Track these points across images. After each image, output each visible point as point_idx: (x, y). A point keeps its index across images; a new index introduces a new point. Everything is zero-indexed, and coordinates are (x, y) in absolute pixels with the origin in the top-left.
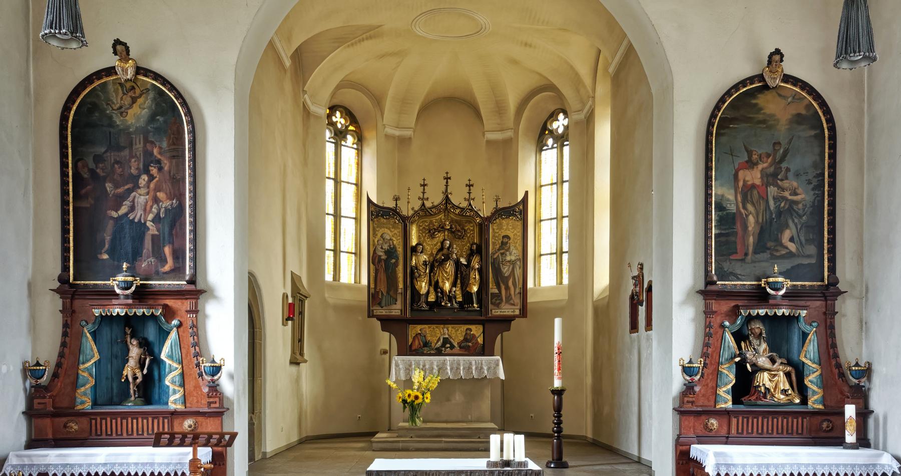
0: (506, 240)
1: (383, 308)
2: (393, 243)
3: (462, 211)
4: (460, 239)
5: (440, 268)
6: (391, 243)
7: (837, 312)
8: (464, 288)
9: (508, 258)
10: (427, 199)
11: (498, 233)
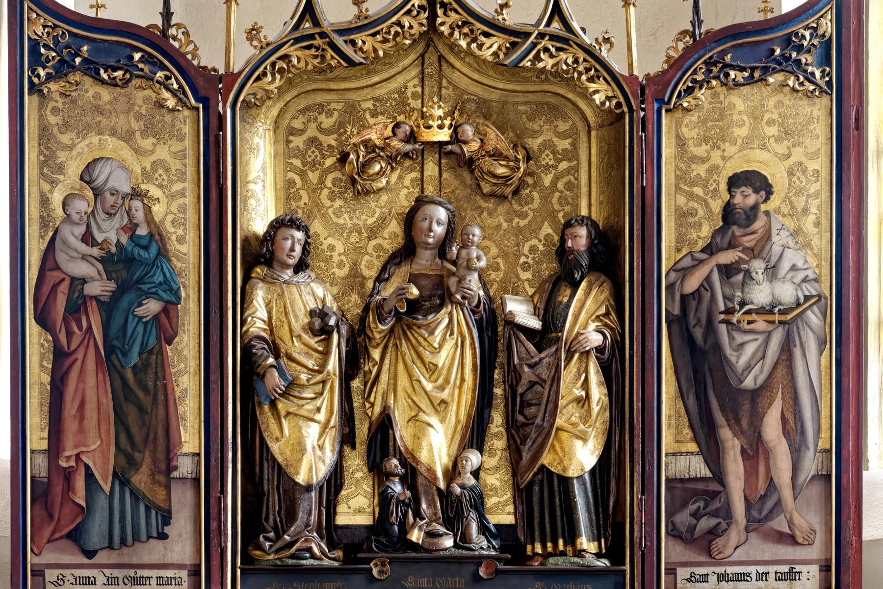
0: (745, 198)
1: (97, 560)
2: (148, 210)
3: (514, 45)
4: (503, 198)
5: (397, 347)
6: (139, 216)
7: (173, 13)
8: (526, 456)
11: (703, 160)
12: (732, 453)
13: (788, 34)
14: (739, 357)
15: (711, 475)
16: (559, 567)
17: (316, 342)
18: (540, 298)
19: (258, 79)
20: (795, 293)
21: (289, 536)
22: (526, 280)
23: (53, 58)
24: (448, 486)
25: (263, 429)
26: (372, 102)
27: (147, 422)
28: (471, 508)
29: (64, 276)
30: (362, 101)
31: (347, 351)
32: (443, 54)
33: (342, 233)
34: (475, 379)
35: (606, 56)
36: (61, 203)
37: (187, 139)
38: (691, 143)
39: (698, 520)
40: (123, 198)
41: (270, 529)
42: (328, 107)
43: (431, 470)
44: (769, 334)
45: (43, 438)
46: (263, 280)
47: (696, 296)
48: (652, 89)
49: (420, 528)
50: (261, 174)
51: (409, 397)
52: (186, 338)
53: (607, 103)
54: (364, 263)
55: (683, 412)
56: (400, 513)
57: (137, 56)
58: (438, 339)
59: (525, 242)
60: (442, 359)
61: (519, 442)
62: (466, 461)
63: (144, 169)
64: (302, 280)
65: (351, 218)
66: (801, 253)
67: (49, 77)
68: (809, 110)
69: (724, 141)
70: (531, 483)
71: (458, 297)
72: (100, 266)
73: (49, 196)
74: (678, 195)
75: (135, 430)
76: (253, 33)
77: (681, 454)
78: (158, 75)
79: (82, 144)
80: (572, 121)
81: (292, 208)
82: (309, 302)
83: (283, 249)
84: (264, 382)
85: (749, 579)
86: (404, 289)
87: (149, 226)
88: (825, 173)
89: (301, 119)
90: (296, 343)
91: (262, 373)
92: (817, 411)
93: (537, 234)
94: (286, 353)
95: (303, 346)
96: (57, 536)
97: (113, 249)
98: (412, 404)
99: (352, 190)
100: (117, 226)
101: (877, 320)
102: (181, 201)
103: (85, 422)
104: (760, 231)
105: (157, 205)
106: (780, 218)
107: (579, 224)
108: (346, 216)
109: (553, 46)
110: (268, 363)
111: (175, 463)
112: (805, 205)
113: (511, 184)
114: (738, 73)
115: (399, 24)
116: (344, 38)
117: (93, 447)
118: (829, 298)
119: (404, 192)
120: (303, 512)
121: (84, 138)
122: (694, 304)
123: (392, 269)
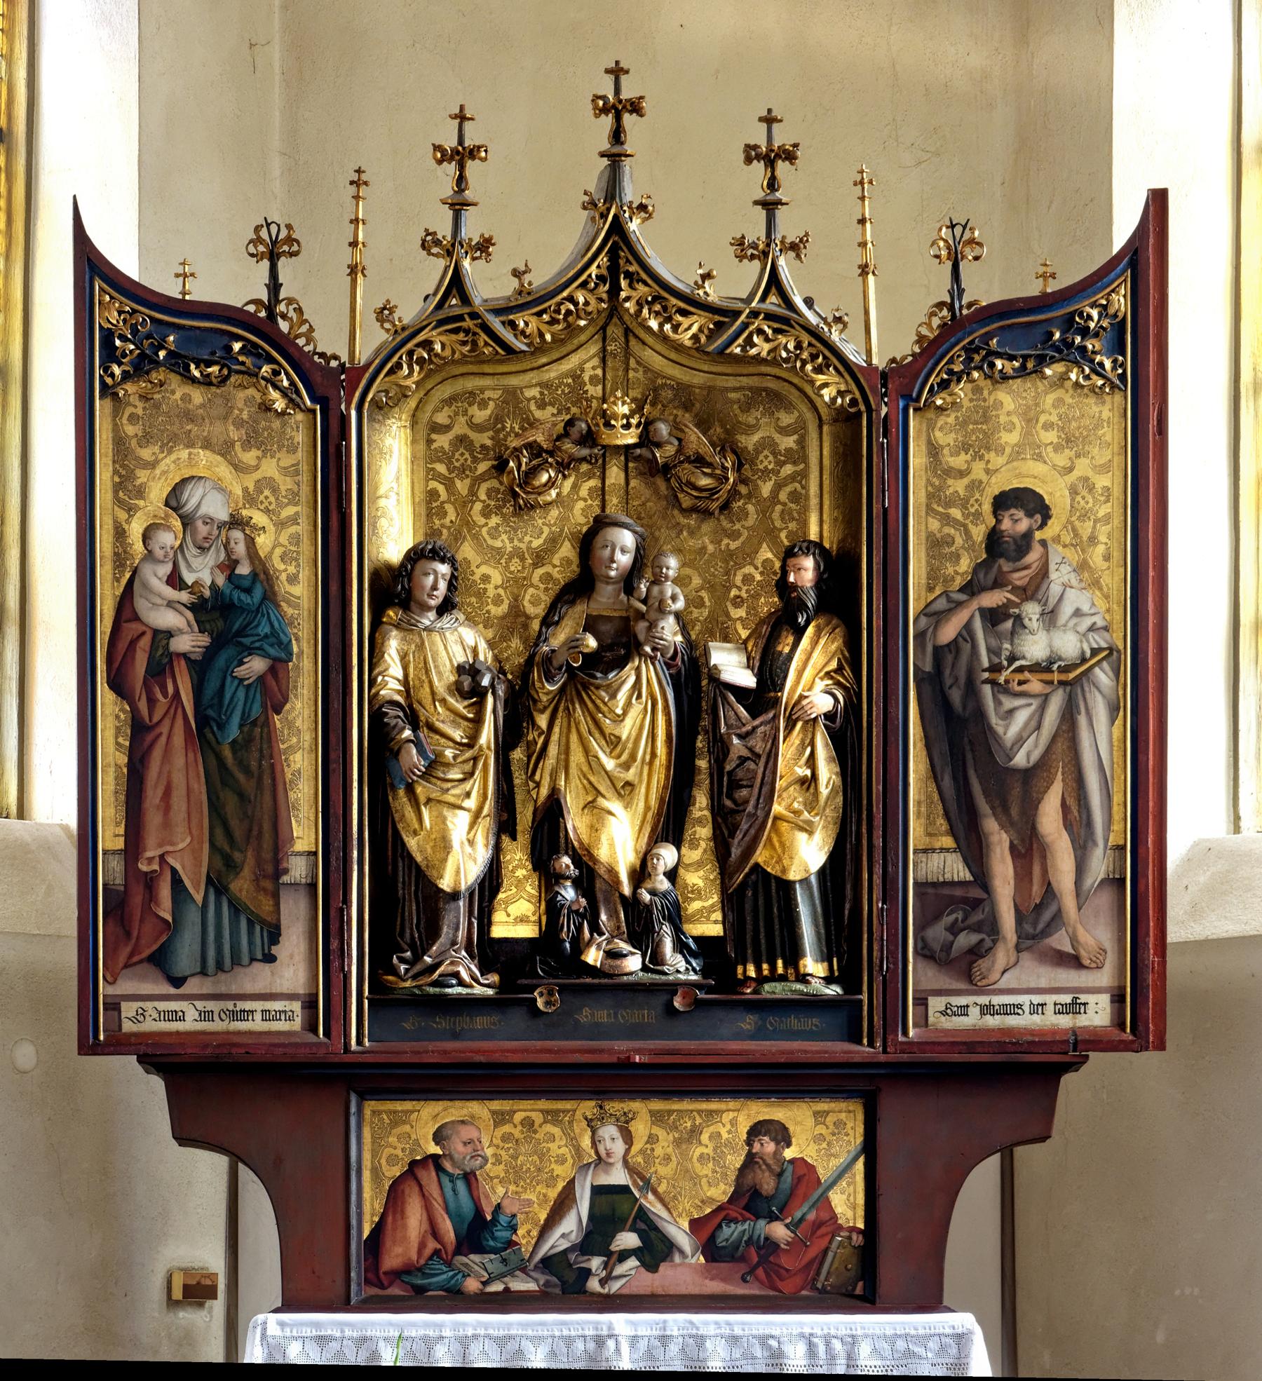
0: (1016, 523)
1: (188, 988)
2: (250, 542)
3: (720, 326)
5: (569, 714)
6: (240, 549)
8: (735, 852)
9: (1035, 647)
10: (484, 247)
11: (962, 474)
12: (998, 850)
13: (1071, 313)
14: (1007, 727)
15: (972, 879)
16: (777, 996)
17: (465, 708)
18: (755, 645)
19: (391, 372)
20: (1079, 645)
21: (430, 957)
22: (738, 619)
23: (131, 352)
24: (634, 892)
25: (397, 819)
26: (538, 389)
27: (250, 813)
28: (664, 919)
29: (144, 628)
30: (526, 387)
31: (504, 716)
32: (631, 327)
33: (500, 559)
34: (669, 754)
35: (837, 339)
36: (140, 536)
37: (300, 450)
38: (946, 451)
39: (955, 935)
40: (219, 527)
41: (406, 947)
42: (481, 396)
43: (612, 872)
44: (1045, 698)
45: (118, 835)
46: (397, 626)
47: (952, 647)
48: (897, 383)
49: (599, 947)
50: (395, 485)
51: (585, 776)
52: (299, 705)
53: (839, 401)
54: (527, 597)
55: (936, 797)
56: (572, 926)
57: (237, 346)
58: (621, 704)
59: (737, 569)
60: (626, 730)
61: (726, 833)
62: (658, 860)
63: (245, 490)
64: (448, 625)
65: (511, 540)
66: (1087, 594)
67: (126, 376)
68: (1098, 410)
69: (988, 449)
70: (744, 884)
71: (648, 649)
72: (189, 615)
73: (126, 526)
74: (929, 518)
75: (234, 823)
76: (384, 313)
77: (934, 850)
78: (263, 370)
79: (167, 461)
80: (799, 411)
81: (436, 527)
82: (457, 655)
83: (423, 588)
84: (398, 760)
85: (1020, 1011)
86: (578, 640)
87: (252, 563)
88: (1117, 492)
89: (447, 411)
90: (439, 709)
91: (396, 748)
92: (1108, 796)
93: (753, 559)
94: (427, 721)
95: (448, 713)
96: (135, 959)
97: (207, 593)
98: (588, 786)
99: (512, 503)
100: (212, 563)
101: (1253, 620)
102: (293, 529)
103: (171, 814)
104: (1034, 566)
105: (262, 536)
106: (1060, 548)
107: (803, 553)
108: (504, 537)
109: (769, 327)
110: (403, 736)
111: (285, 865)
112: (1092, 532)
113: (718, 499)
114: (1006, 362)
115: (571, 299)
116: (503, 318)
117: (181, 846)
118: (1123, 651)
119: (581, 504)
120: (449, 926)
121: (170, 452)
122: (949, 658)
123: (563, 610)
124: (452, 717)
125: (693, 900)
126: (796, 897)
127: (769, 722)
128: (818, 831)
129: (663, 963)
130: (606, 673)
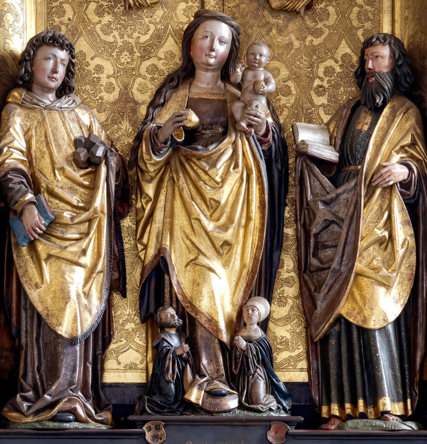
4: (295, 13)
8: (321, 305)
18: (337, 126)
21: (50, 395)
22: (321, 106)
24: (232, 339)
25: (20, 274)
28: (259, 364)
33: (112, 52)
41: (28, 388)
43: (212, 321)
46: (21, 105)
49: (200, 387)
51: (188, 237)
54: (136, 86)
56: (177, 370)
58: (220, 172)
59: (319, 63)
62: (253, 311)
64: (66, 106)
65: (122, 36)
71: (244, 124)
83: (44, 70)
84: (22, 221)
90: (58, 177)
94: (47, 187)
95: (66, 180)
98: (190, 246)
99: (123, 3)
108: (115, 33)
120: (66, 368)
123: (168, 93)
124: (70, 183)
125: (281, 350)
126: (376, 344)
127: (351, 190)
128: (395, 287)
129: (257, 402)
130: (206, 146)
